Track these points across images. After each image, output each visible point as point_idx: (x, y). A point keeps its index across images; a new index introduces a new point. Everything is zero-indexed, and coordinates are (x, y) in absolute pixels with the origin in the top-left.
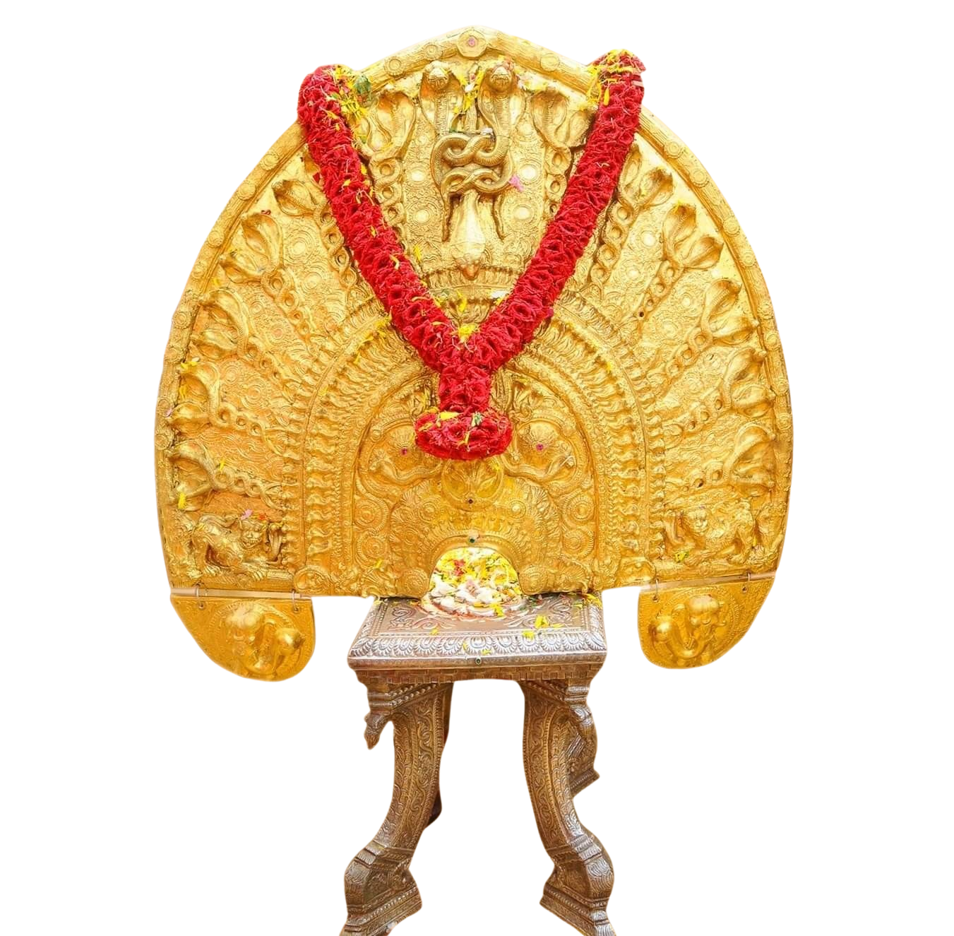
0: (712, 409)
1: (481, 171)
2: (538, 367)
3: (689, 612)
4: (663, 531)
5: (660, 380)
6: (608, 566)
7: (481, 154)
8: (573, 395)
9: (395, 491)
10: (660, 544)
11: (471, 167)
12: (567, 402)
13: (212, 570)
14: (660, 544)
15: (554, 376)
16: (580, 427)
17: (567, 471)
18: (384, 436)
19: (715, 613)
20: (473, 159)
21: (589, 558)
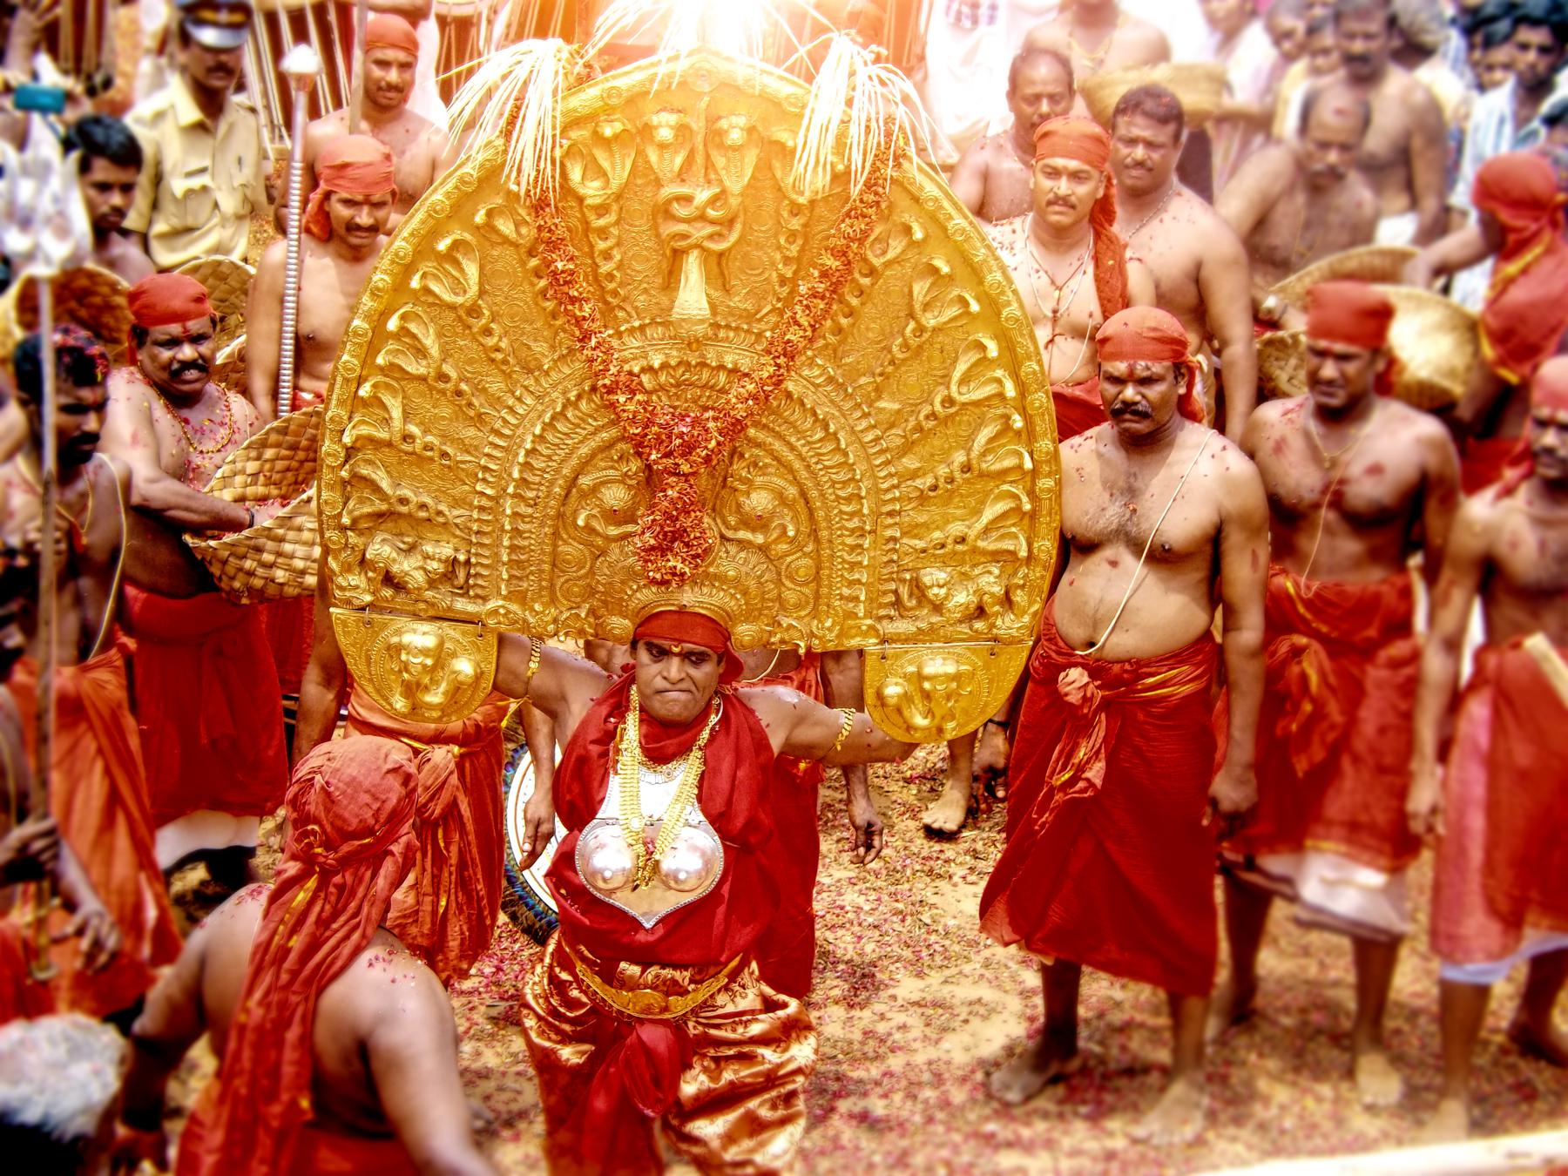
0: (957, 475)
1: (710, 229)
2: (761, 436)
3: (920, 677)
4: (896, 592)
5: (899, 441)
6: (829, 629)
7: (711, 213)
8: (797, 465)
9: (600, 541)
10: (893, 604)
11: (699, 225)
12: (791, 471)
13: (388, 593)
14: (893, 604)
15: (777, 445)
16: (803, 494)
17: (744, 632)
18: (594, 490)
19: (957, 677)
20: (702, 217)
21: (806, 620)
